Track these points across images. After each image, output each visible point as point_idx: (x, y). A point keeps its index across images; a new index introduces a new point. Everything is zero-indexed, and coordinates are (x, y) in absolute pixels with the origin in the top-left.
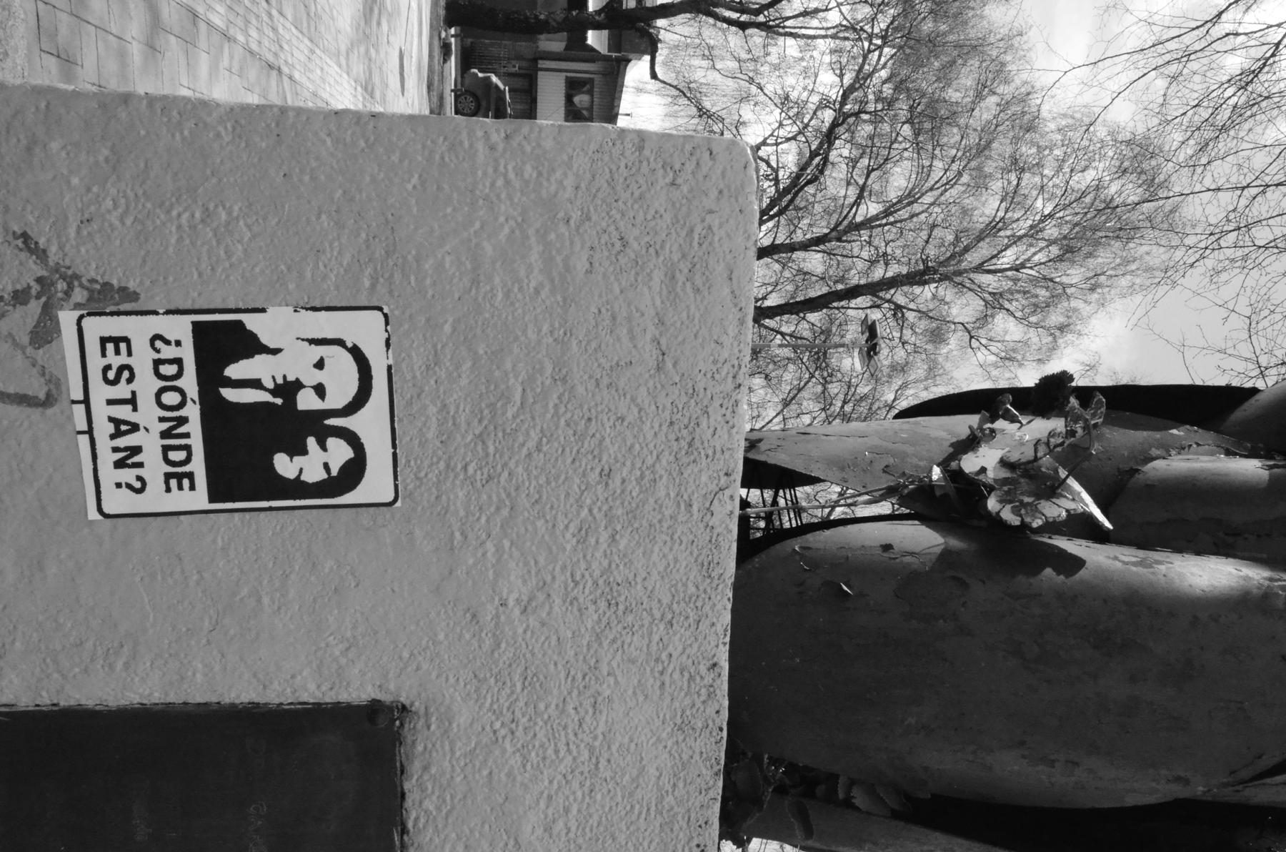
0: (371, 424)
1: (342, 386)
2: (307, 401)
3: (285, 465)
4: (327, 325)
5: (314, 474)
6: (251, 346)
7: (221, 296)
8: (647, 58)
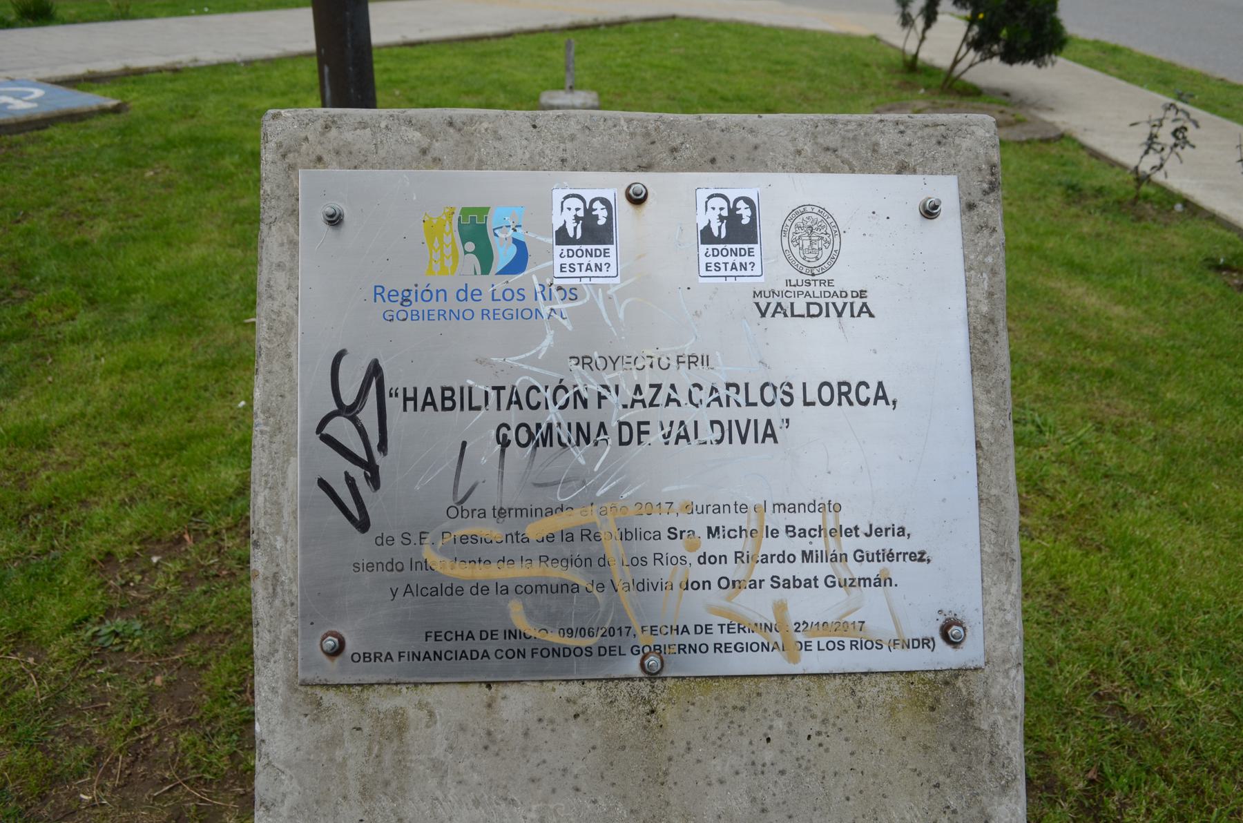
0: (588, 195)
1: (720, 202)
2: (581, 214)
3: (745, 221)
4: (557, 206)
5: (749, 212)
6: (708, 229)
7: (694, 237)
8: (596, 103)
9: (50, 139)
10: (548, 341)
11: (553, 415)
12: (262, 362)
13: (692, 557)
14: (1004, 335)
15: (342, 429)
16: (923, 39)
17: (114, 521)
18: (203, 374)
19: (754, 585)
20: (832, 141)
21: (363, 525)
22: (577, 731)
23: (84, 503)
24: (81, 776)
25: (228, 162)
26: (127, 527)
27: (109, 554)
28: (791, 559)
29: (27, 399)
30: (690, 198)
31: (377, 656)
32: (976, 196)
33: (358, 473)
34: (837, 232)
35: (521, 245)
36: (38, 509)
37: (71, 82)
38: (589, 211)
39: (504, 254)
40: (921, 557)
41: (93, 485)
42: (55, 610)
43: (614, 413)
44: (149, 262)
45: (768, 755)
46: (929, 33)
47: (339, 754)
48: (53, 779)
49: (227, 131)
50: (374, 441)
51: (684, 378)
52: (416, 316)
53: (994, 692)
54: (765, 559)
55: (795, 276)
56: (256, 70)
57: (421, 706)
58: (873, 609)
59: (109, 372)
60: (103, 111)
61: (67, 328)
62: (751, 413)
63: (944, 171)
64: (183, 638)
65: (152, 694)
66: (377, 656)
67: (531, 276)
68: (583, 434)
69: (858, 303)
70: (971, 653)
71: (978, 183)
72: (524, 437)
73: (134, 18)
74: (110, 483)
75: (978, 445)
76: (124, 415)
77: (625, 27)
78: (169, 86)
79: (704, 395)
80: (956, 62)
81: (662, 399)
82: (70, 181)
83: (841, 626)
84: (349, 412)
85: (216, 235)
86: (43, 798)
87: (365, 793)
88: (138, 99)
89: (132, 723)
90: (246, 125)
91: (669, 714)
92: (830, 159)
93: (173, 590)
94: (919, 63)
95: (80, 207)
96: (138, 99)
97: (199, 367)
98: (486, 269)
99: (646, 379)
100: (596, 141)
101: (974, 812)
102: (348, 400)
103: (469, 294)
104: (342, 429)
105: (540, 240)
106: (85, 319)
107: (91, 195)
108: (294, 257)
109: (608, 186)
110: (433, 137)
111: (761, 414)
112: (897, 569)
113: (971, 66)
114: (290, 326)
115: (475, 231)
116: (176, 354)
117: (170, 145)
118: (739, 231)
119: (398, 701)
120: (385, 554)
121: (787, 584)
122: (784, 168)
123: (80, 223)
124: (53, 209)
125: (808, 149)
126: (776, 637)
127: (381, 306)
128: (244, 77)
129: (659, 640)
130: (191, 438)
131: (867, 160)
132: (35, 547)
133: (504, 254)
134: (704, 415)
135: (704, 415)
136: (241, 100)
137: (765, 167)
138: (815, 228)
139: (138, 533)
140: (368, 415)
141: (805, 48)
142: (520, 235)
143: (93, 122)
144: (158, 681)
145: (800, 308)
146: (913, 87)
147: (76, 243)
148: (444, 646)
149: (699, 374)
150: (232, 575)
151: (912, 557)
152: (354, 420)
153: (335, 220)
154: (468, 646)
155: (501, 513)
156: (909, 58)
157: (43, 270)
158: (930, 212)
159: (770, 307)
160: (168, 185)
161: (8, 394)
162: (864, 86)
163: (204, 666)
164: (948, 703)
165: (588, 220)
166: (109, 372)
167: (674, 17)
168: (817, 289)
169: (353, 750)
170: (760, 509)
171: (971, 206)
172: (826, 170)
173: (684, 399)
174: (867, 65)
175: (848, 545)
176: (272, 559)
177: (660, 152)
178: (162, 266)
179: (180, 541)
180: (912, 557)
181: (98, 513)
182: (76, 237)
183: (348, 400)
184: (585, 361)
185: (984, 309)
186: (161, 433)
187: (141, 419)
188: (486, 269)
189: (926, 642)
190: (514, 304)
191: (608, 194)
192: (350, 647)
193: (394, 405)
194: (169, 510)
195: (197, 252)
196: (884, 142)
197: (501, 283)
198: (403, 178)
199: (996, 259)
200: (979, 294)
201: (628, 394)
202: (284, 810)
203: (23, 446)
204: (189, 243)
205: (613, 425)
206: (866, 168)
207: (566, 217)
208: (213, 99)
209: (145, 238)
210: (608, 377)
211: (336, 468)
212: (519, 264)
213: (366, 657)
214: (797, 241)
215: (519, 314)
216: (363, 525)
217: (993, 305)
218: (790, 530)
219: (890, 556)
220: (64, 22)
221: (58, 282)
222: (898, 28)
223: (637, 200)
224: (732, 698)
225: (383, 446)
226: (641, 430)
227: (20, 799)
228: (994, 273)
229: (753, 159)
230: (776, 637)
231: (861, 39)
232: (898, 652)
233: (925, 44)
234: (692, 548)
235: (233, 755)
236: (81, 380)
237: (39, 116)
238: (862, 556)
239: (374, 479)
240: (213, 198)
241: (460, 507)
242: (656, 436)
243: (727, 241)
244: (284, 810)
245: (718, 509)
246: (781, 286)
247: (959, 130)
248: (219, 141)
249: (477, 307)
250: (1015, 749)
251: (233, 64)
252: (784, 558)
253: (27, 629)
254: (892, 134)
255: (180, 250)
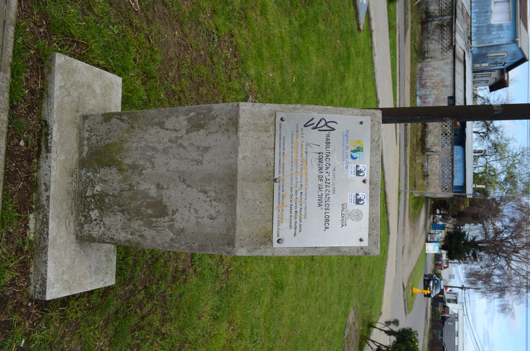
0: (365, 172)
6: (358, 195)
9: (350, 7)
10: (338, 163)
11: (324, 163)
12: (336, 108)
13: (297, 189)
14: (337, 254)
15: (323, 123)
16: (381, 330)
17: (242, 37)
18: (279, 62)
19: (291, 201)
20: (375, 221)
21: (305, 126)
22: (264, 165)
23: (246, 27)
24: (181, 31)
25: (342, 68)
26: (240, 41)
27: (233, 36)
28: (296, 209)
29: (274, 8)
30: (364, 193)
31: (280, 127)
32: (364, 250)
33: (315, 125)
34: (358, 221)
35: (356, 158)
36: (245, 14)
37: (368, 12)
38: (362, 172)
39: (355, 155)
40: (295, 235)
41: (251, 30)
42: (220, 21)
43: (324, 174)
44: (312, 44)
45: (258, 203)
46: (383, 332)
47: (262, 119)
48: (182, 24)
49: (352, 67)
50: (321, 129)
51: (331, 189)
52: (343, 138)
53: (268, 249)
54: (296, 203)
55: (349, 212)
56: (372, 76)
57: (271, 135)
58: (285, 225)
59: (281, 33)
60: (359, 25)
61: (294, 19)
62: (324, 202)
63: (369, 243)
64: (211, 59)
65: (199, 51)
66: (280, 127)
67: (350, 160)
68: (321, 169)
69: (344, 224)
70: (276, 245)
71: (366, 250)
72: (321, 157)
73: (389, 31)
74: (251, 35)
75: (316, 247)
76: (269, 38)
77: (386, 214)
78: (366, 46)
79: (327, 193)
80: (373, 341)
81: (327, 184)
82: (337, 15)
83: (282, 218)
84: (326, 124)
85: (319, 65)
86: (177, 21)
87: (255, 124)
88: (362, 36)
89: (193, 45)
90: (354, 74)
91: (267, 183)
92: (371, 220)
93: (223, 56)
94: (372, 329)
95: (329, 19)
96: (362, 36)
97: (281, 61)
98: (352, 151)
99: (331, 181)
100: (375, 174)
101: (244, 244)
102: (328, 124)
103: (347, 148)
104: (323, 123)
105: (357, 162)
106: (296, 24)
107: (332, 23)
108: (355, 115)
109: (367, 176)
110: (376, 142)
111: (324, 204)
112: (293, 230)
113: (372, 348)
114: (342, 114)
115: (359, 150)
116: (285, 54)
117: (348, 48)
118: (358, 201)
119: (272, 131)
120: (300, 130)
121: (291, 208)
122: (370, 211)
123: (324, 20)
124: (328, 10)
125: (373, 216)
126: (281, 205)
127: (345, 131)
128: (369, 72)
129: (281, 182)
130: (262, 59)
131: (371, 228)
132: (235, 14)
133: (355, 155)
134: (324, 192)
135: (324, 192)
136: (361, 72)
137: (370, 207)
138: (358, 216)
139: (238, 44)
140: (325, 128)
141: (377, 284)
142: (358, 158)
143: (355, 22)
144: (202, 52)
145: (343, 212)
146: (363, 325)
147: (318, 19)
148: (282, 140)
149: (331, 192)
150: (226, 73)
151: (295, 233)
152: (324, 125)
153: (361, 123)
154: (282, 145)
155: (306, 152)
156: (373, 324)
157: (310, 9)
158: (361, 240)
159: (344, 206)
160: (335, 48)
161: (276, 2)
162: (364, 305)
163: (205, 65)
164: (266, 240)
165: (361, 171)
166: (281, 33)
167: (389, 234)
168: (347, 216)
169: (263, 122)
170: (305, 203)
171: (362, 249)
172: (369, 219)
173: (327, 189)
174: (371, 307)
175: (298, 220)
176: (299, 109)
177: (373, 186)
178: (311, 48)
179: (235, 57)
180: (295, 233)
181: (244, 32)
182: (320, 19)
183: (328, 124)
184: (334, 170)
185: (342, 250)
186: (264, 50)
187: (268, 43)
188: (352, 151)
189: (278, 235)
190: (345, 157)
191: (365, 176)
192: (282, 122)
193: (327, 133)
194: (244, 53)
195: (314, 59)
196: (374, 231)
197: (349, 154)
198: (369, 136)
199: (352, 253)
200: (345, 249)
201: (328, 178)
202: (252, 108)
203: (262, 7)
204: (317, 57)
205: (322, 174)
206: (370, 227)
207: (361, 167)
208: (362, 62)
209: (319, 42)
210: (331, 174)
211: (316, 121)
212: (352, 158)
213: (280, 125)
214: (356, 212)
215: (343, 157)
216: (305, 126)
217: (343, 252)
218: (301, 209)
219: (295, 229)
220: (388, 7)
221: (307, 15)
222: (385, 320)
223: (364, 181)
224: (269, 196)
225: (320, 130)
226: (321, 180)
227: (177, 15)
228: (349, 252)
229: (371, 205)
230: (281, 205)
231: (381, 308)
232: (277, 230)
233: (379, 331)
234: (298, 189)
235: (184, 74)
236: (279, 24)
237: (357, 3)
238: (296, 223)
239: (313, 128)
240: (331, 64)
241: (308, 144)
242: (320, 183)
243: (356, 199)
244: (252, 108)
245: (306, 194)
246: (347, 209)
247: (377, 247)
248: (349, 65)
249: (345, 149)
250: (257, 253)
251: (374, 69)
252: (296, 207)
253: (216, 14)
254: (376, 233)
255: (315, 53)
